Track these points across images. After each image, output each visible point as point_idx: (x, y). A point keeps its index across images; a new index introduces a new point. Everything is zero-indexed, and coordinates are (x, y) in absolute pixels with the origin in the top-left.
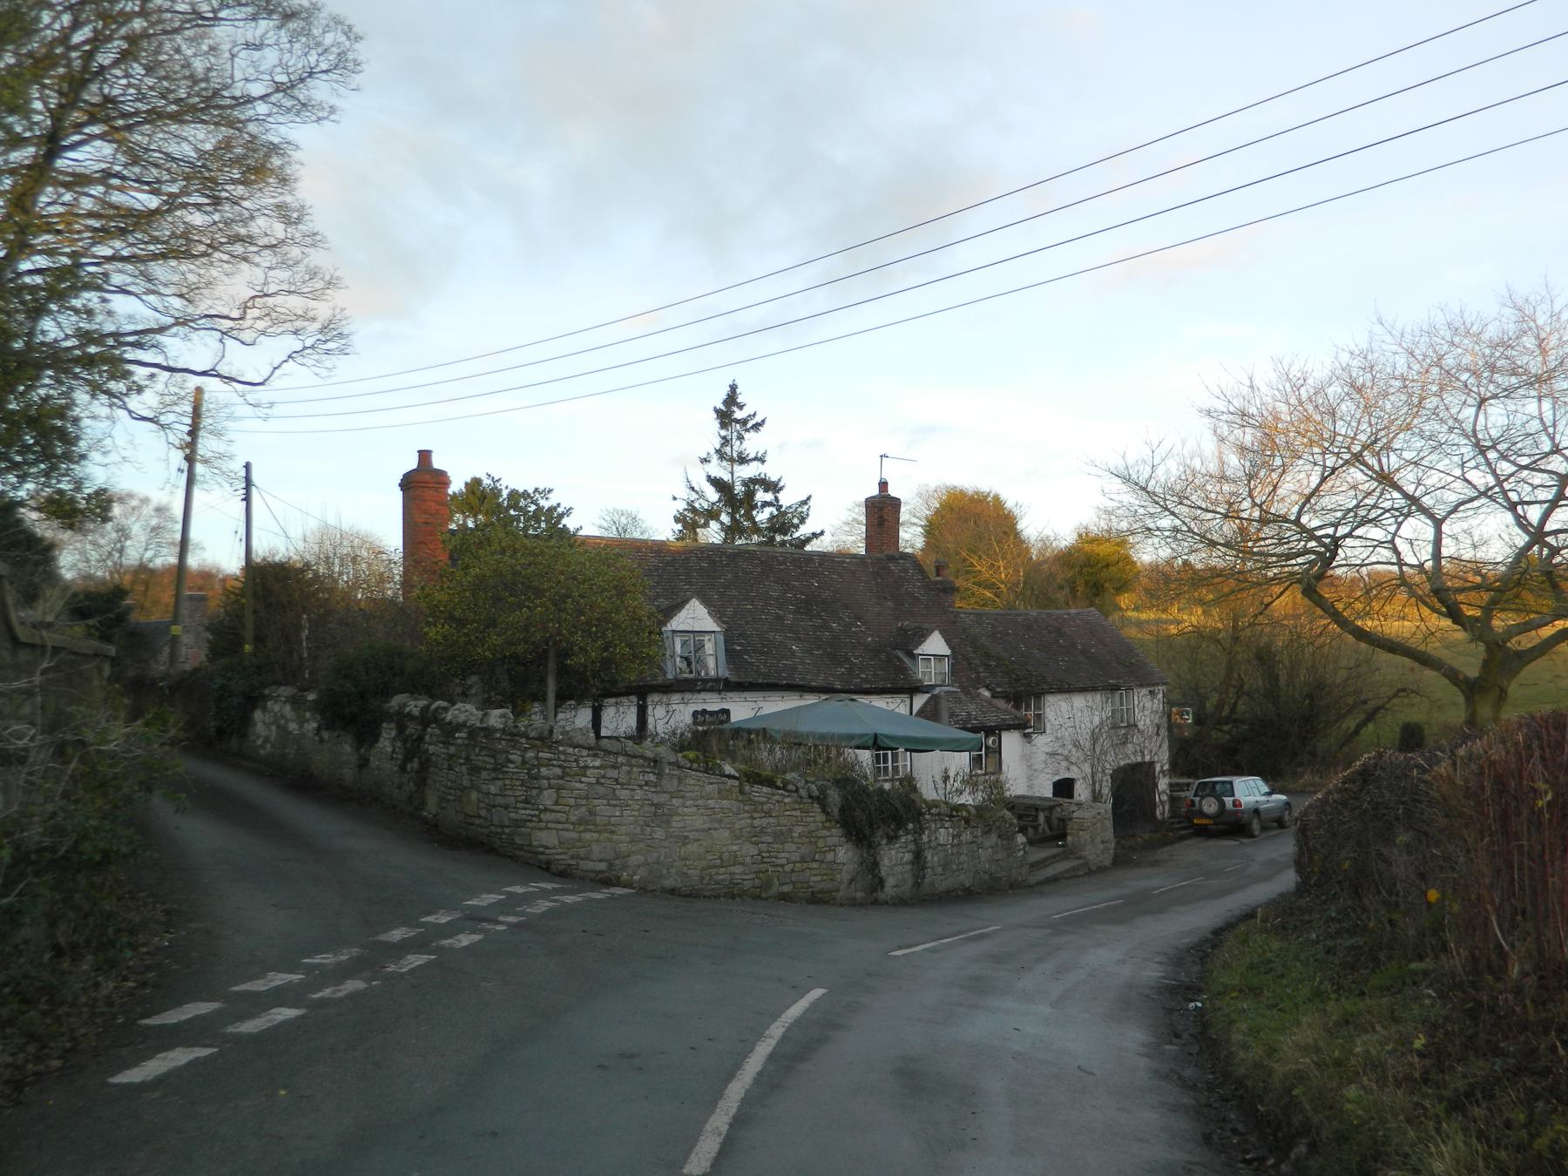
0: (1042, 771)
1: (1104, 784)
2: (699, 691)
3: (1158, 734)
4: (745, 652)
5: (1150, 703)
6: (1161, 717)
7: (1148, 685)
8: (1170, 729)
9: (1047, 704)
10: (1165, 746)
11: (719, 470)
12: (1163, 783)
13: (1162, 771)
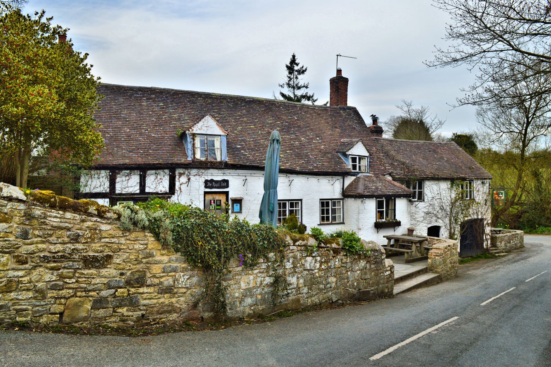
0: (422, 222)
1: (456, 229)
2: (209, 168)
3: (486, 204)
4: (243, 149)
5: (482, 188)
6: (488, 196)
7: (481, 179)
8: (492, 204)
9: (426, 186)
10: (490, 210)
11: (288, 92)
12: (488, 230)
13: (488, 224)
